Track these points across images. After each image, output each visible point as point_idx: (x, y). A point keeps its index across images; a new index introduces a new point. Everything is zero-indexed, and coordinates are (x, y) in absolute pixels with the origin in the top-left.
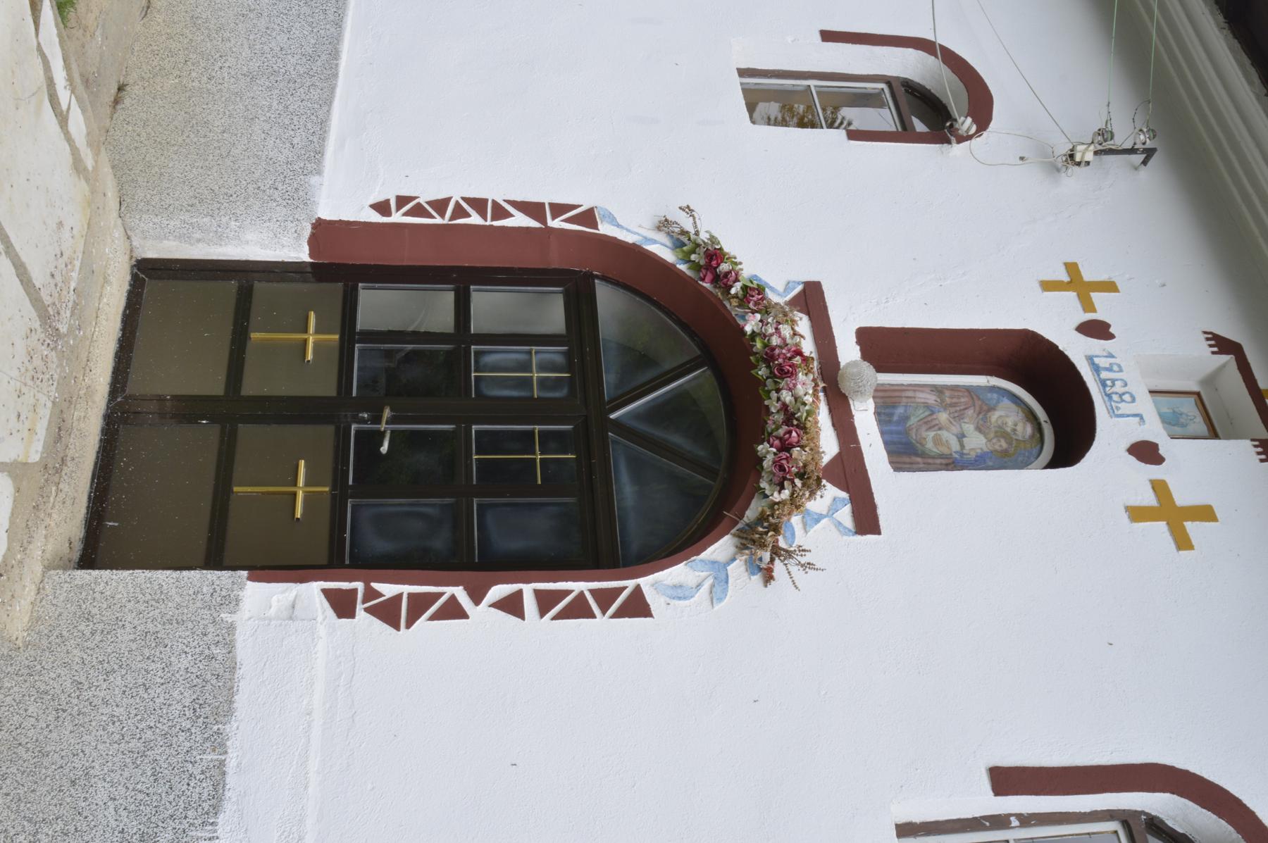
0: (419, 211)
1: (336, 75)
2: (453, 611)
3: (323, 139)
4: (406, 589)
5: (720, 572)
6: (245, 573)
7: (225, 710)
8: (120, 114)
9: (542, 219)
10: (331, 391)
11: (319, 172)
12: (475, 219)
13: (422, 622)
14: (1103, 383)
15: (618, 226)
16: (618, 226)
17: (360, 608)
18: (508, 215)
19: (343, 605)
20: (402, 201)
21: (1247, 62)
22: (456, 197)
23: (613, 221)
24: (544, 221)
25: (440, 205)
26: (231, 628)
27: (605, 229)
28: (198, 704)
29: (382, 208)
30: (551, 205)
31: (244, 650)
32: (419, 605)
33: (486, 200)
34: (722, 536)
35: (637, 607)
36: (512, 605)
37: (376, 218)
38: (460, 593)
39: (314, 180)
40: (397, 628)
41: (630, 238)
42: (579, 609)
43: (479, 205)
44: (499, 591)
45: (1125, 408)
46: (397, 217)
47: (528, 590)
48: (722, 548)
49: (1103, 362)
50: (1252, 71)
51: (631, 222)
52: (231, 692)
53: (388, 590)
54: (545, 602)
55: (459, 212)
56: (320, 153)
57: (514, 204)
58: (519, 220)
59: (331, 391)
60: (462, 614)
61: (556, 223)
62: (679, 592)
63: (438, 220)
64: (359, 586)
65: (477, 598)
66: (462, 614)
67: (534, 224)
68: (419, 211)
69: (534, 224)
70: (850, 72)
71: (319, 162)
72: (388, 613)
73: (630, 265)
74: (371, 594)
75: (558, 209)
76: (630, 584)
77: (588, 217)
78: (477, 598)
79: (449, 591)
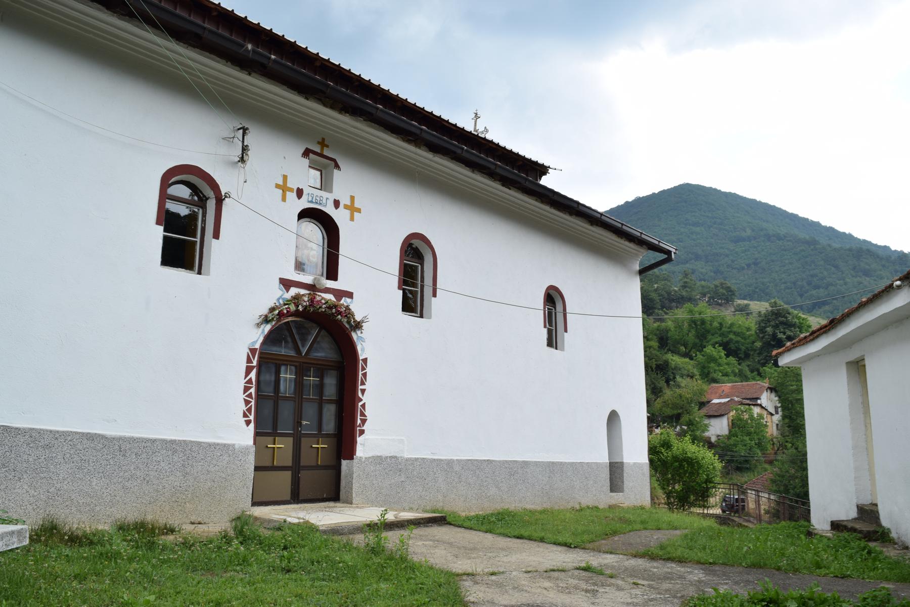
0: (249, 410)
1: (184, 441)
2: (363, 406)
3: (218, 444)
5: (360, 338)
8: (206, 520)
9: (253, 367)
10: (291, 439)
11: (234, 445)
12: (253, 390)
18: (251, 379)
19: (362, 432)
20: (245, 415)
21: (208, 54)
23: (255, 342)
25: (247, 402)
27: (257, 346)
28: (380, 464)
29: (248, 423)
31: (370, 455)
32: (363, 414)
35: (365, 361)
36: (363, 391)
37: (252, 425)
38: (360, 404)
39: (236, 447)
41: (261, 339)
42: (365, 375)
43: (246, 389)
44: (360, 394)
45: (324, 201)
46: (252, 417)
47: (360, 387)
48: (354, 335)
49: (310, 199)
50: (212, 56)
51: (256, 336)
53: (359, 422)
55: (250, 396)
56: (225, 445)
57: (246, 377)
58: (253, 375)
59: (291, 439)
60: (364, 404)
61: (255, 363)
62: (363, 350)
63: (253, 403)
66: (364, 404)
67: (254, 371)
68: (249, 410)
69: (254, 371)
71: (229, 445)
72: (364, 421)
73: (270, 339)
74: (360, 426)
77: (253, 351)
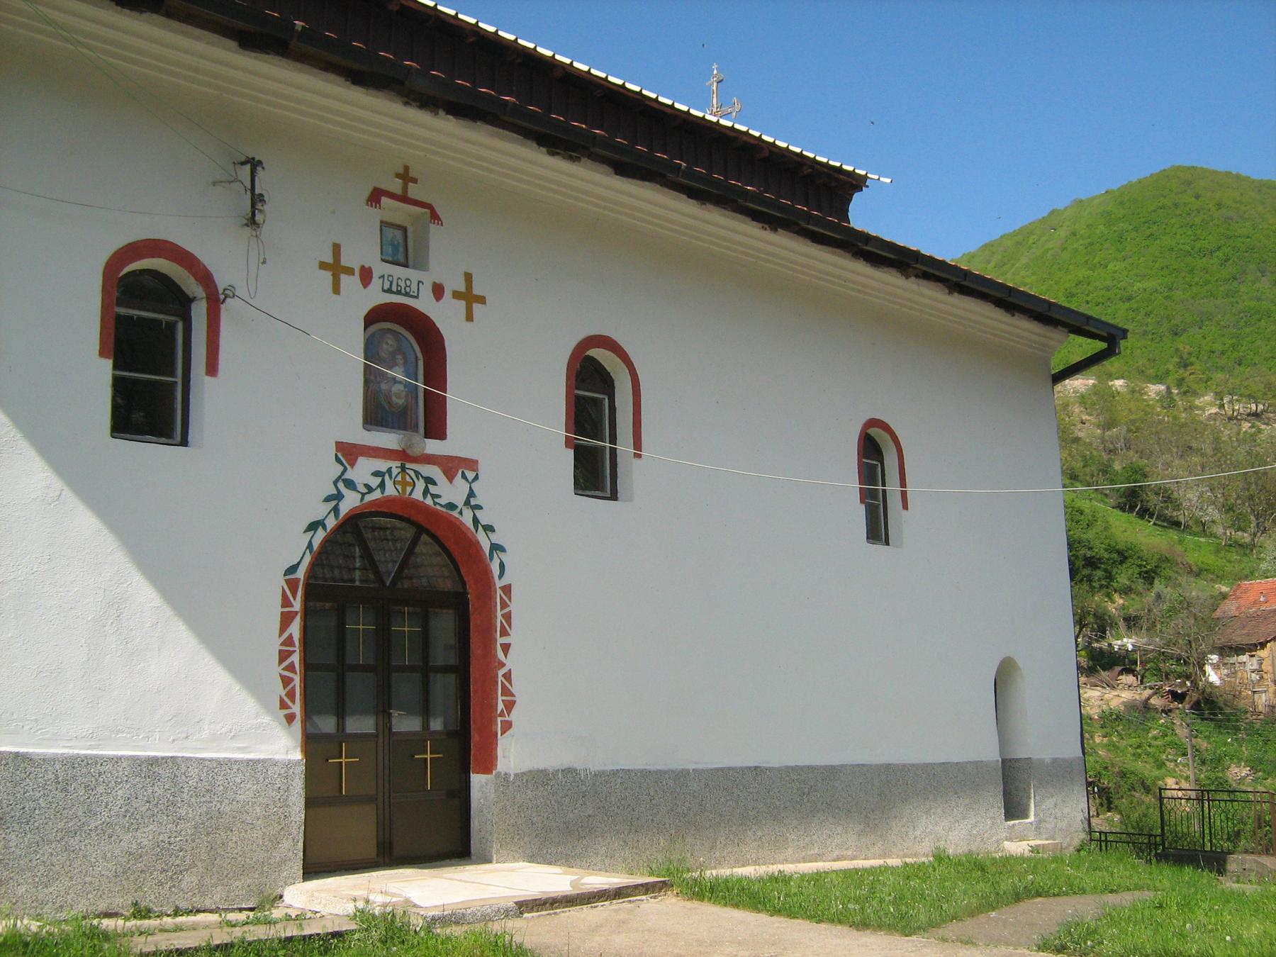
2: (508, 676)
4: (500, 698)
6: (477, 779)
7: (543, 773)
10: (370, 810)
12: (296, 658)
13: (514, 690)
14: (398, 293)
15: (299, 564)
16: (299, 564)
17: (507, 718)
22: (279, 670)
24: (296, 613)
25: (286, 681)
26: (516, 775)
30: (283, 606)
32: (506, 692)
33: (280, 651)
34: (400, 733)
36: (506, 648)
38: (501, 673)
40: (514, 702)
42: (508, 617)
43: (283, 656)
44: (500, 655)
52: (539, 771)
53: (501, 706)
54: (504, 633)
55: (291, 668)
58: (295, 629)
59: (370, 810)
64: (499, 719)
65: (503, 665)
68: (291, 695)
70: (190, 432)
72: (510, 706)
75: (286, 602)
76: (499, 592)
78: (503, 665)
79: (500, 678)
